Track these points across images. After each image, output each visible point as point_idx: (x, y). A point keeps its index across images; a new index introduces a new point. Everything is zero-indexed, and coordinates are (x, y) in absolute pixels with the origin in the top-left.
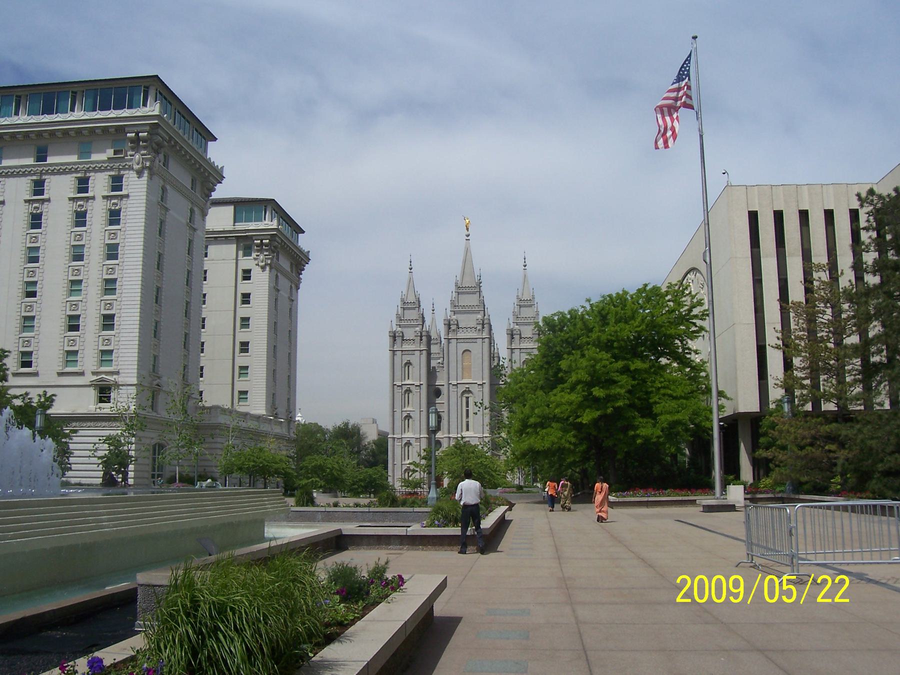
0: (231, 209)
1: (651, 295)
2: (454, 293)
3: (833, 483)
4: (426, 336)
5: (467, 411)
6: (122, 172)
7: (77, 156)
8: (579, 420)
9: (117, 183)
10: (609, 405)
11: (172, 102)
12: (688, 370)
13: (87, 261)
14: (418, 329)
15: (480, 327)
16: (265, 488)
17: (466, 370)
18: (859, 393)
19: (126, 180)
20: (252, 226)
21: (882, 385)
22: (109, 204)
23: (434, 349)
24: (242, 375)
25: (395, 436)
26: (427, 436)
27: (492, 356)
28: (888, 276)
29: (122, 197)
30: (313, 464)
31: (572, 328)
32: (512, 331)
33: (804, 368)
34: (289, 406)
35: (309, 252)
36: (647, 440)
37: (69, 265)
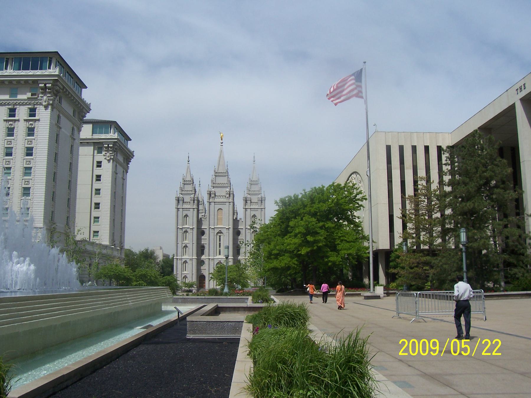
0: (90, 126)
1: (337, 188)
2: (213, 175)
3: (426, 285)
4: (197, 200)
5: (220, 243)
6: (36, 106)
7: (9, 96)
8: (300, 252)
9: (32, 112)
10: (315, 245)
11: (64, 67)
12: (352, 226)
13: (15, 157)
14: (192, 196)
15: (228, 196)
16: (110, 285)
17: (219, 220)
18: (440, 243)
19: (38, 111)
20: (103, 136)
21: (451, 239)
22: (28, 124)
23: (201, 207)
24: (95, 222)
25: (178, 258)
26: (197, 258)
27: (234, 212)
28: (455, 189)
29: (35, 120)
30: (140, 274)
31: (295, 205)
32: (246, 198)
33: (413, 229)
34: (121, 240)
35: (134, 151)
36: (334, 263)
37: (4, 158)
